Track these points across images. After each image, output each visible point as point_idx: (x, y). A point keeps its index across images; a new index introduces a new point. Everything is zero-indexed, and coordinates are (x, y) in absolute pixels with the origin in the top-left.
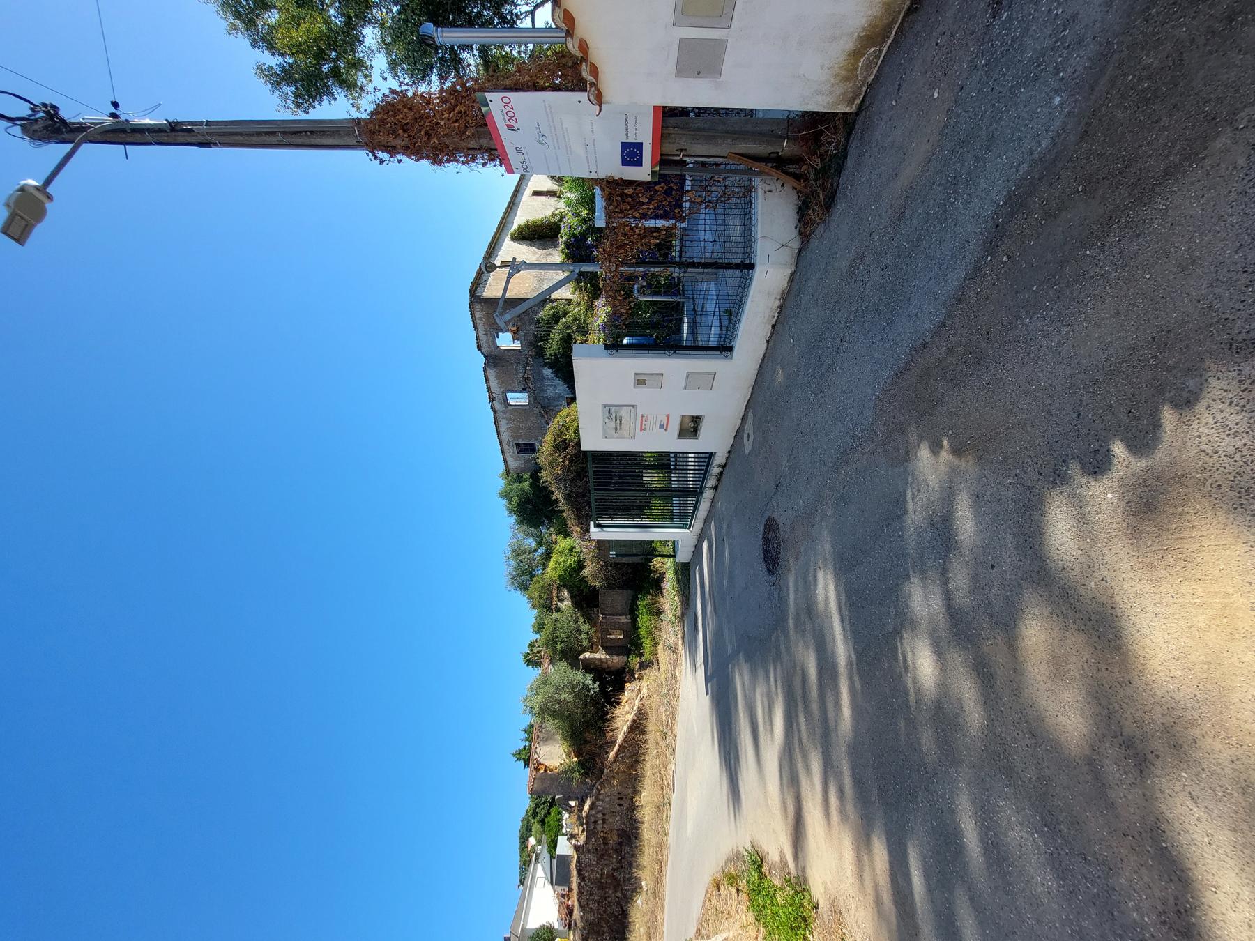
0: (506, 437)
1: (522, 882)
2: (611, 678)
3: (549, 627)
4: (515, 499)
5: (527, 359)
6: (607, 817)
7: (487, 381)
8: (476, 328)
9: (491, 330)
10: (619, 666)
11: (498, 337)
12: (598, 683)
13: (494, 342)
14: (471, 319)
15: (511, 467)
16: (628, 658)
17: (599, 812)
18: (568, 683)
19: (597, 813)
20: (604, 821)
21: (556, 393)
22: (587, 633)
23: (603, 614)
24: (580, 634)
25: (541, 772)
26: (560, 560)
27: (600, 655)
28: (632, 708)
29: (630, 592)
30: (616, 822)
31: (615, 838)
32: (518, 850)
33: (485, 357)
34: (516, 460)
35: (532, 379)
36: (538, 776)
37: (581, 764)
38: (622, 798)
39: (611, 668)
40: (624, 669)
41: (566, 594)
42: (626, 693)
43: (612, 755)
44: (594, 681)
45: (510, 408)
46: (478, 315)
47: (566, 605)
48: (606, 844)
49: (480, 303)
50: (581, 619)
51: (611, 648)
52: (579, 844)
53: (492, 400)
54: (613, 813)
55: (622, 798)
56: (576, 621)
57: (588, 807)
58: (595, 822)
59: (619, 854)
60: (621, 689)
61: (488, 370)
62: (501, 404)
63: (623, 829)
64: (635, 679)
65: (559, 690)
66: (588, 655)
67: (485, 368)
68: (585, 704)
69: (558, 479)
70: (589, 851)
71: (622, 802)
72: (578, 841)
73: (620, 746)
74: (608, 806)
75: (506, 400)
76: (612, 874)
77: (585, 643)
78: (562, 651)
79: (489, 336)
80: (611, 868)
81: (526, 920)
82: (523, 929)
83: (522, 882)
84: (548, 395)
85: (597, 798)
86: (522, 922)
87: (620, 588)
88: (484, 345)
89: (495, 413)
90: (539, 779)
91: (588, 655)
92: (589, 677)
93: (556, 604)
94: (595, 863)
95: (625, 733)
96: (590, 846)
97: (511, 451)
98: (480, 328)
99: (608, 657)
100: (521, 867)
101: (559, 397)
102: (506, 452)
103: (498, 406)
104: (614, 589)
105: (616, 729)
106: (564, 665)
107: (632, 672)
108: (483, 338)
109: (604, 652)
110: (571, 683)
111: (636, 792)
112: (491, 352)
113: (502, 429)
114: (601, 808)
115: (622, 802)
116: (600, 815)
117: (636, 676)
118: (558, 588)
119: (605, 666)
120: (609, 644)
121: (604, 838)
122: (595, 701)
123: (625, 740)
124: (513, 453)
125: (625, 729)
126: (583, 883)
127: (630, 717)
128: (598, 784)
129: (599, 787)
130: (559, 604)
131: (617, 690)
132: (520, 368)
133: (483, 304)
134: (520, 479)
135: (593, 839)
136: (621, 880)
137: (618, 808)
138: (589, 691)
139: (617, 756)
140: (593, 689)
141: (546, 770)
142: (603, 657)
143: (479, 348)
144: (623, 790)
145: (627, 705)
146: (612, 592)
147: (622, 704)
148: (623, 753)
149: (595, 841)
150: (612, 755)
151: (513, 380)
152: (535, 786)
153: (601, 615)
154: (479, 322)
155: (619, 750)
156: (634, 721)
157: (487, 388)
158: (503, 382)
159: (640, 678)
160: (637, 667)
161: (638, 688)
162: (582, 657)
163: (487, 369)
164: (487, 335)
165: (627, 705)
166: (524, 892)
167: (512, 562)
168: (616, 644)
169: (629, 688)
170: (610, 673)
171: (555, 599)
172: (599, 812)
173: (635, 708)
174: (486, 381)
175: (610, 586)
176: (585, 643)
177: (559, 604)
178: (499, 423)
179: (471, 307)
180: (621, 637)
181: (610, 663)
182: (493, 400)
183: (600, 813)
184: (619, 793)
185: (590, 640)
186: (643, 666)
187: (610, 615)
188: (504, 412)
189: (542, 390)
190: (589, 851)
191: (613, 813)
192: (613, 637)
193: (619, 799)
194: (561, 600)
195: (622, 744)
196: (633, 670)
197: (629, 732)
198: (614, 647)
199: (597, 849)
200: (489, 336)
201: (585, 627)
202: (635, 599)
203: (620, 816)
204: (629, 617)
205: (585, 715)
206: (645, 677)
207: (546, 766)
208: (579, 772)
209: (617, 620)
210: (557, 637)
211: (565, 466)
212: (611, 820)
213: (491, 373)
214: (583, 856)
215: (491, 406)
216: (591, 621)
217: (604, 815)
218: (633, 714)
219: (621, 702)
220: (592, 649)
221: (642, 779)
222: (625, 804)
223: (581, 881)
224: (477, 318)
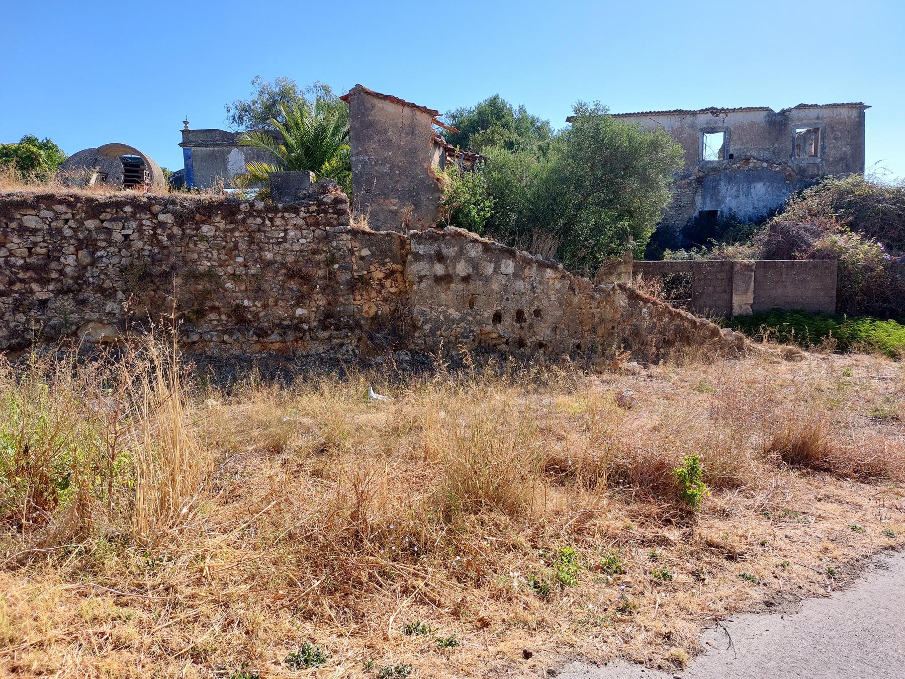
5: (780, 164)
6: (455, 286)
14: (814, 104)
19: (471, 261)
20: (445, 279)
21: (725, 197)
32: (543, 118)
33: (783, 112)
35: (746, 168)
46: (844, 112)
53: (713, 111)
61: (766, 113)
62: (707, 123)
67: (768, 109)
69: (40, 155)
71: (508, 320)
75: (713, 131)
79: (816, 121)
84: (723, 187)
88: (802, 113)
89: (694, 113)
98: (826, 113)
101: (718, 200)
103: (702, 119)
108: (813, 113)
112: (793, 121)
115: (508, 320)
132: (766, 155)
133: (857, 119)
134: (459, 128)
135: (365, 252)
137: (488, 313)
143: (801, 107)
144: (549, 319)
148: (651, 315)
149: (362, 258)
151: (747, 143)
154: (835, 112)
158: (744, 130)
164: (818, 118)
178: (673, 118)
182: (713, 113)
184: (537, 313)
188: (692, 126)
189: (730, 180)
200: (816, 121)
203: (463, 319)
213: (761, 117)
214: (300, 222)
217: (466, 279)
222: (500, 327)
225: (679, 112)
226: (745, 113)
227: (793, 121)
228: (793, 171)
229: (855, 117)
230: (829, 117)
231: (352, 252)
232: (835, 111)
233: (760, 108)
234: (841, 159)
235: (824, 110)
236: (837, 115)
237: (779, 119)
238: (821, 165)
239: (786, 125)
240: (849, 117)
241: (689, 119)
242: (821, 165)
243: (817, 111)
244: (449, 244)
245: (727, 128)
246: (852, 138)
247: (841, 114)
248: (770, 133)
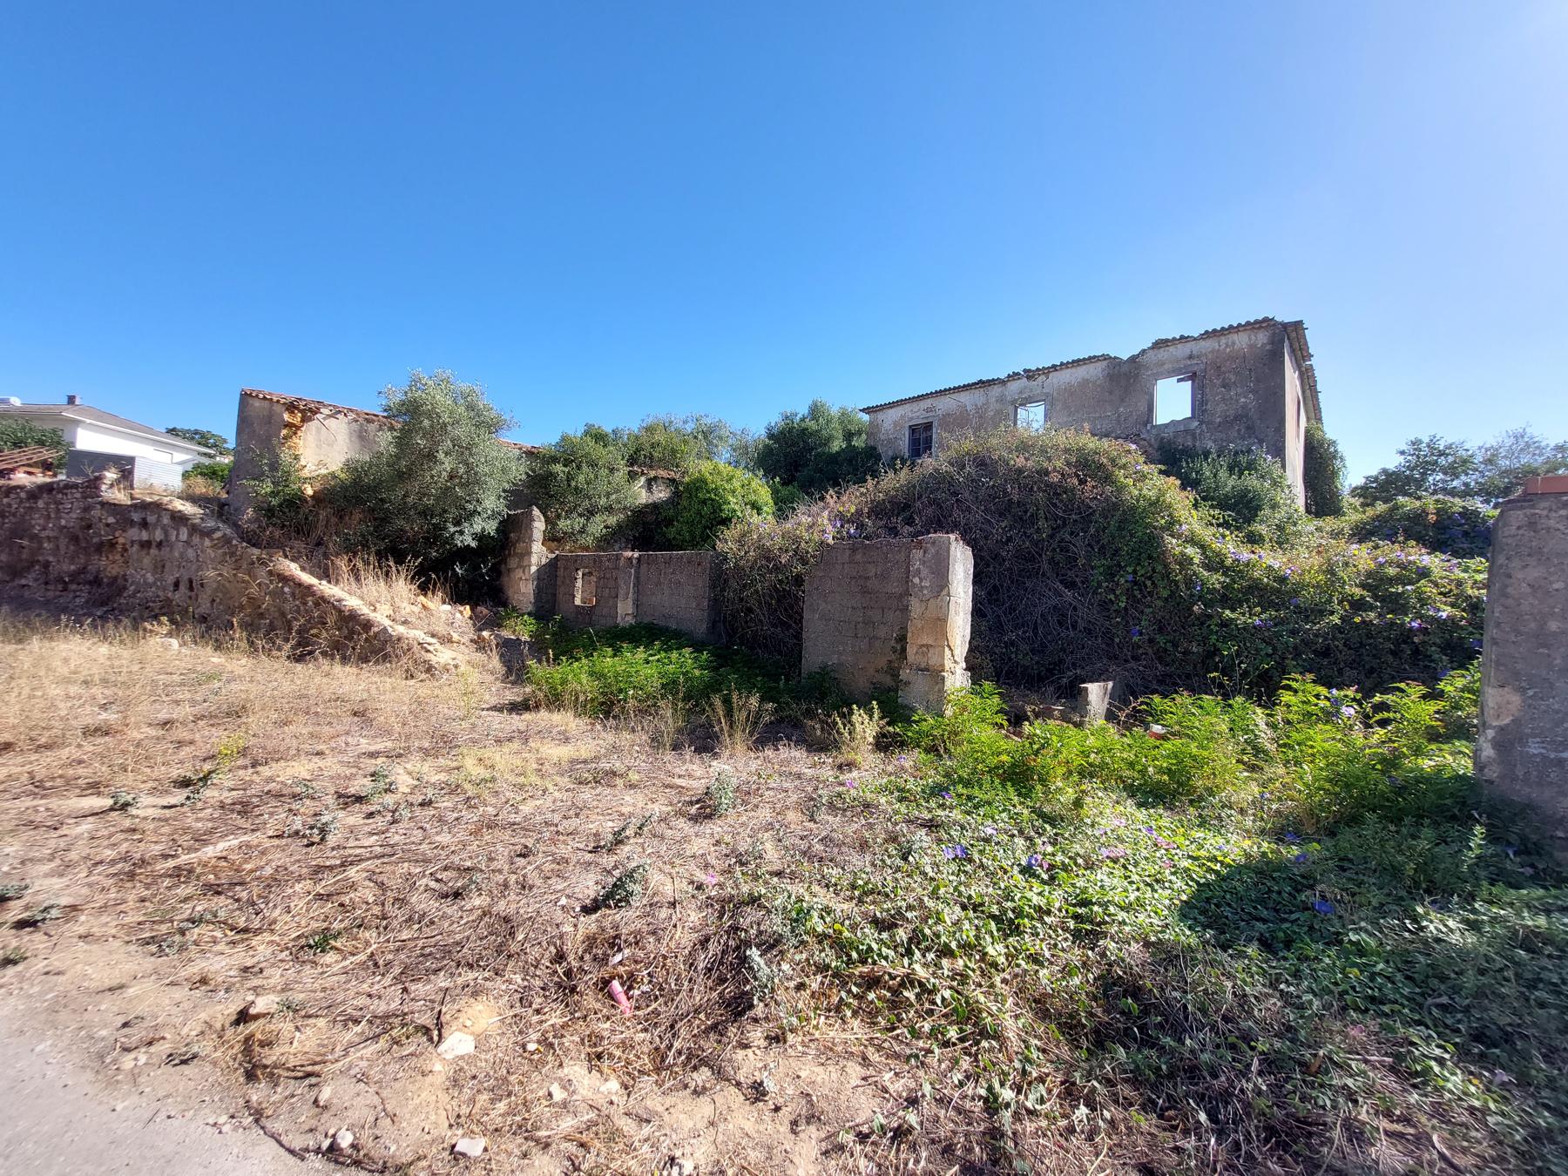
0: (946, 405)
1: (172, 432)
2: (482, 576)
3: (598, 451)
4: (812, 425)
6: (153, 551)
7: (1077, 363)
8: (1207, 335)
9: (1202, 366)
10: (510, 593)
11: (1179, 380)
12: (474, 544)
13: (1170, 374)
15: (880, 416)
16: (529, 614)
17: (166, 533)
18: (476, 474)
20: (146, 545)
22: (582, 531)
23: (639, 559)
24: (581, 515)
25: (286, 416)
26: (736, 484)
27: (539, 553)
28: (405, 623)
29: (701, 629)
30: (142, 573)
31: (114, 570)
33: (1133, 359)
34: (896, 424)
36: (277, 408)
37: (294, 502)
38: (191, 588)
39: (508, 576)
40: (505, 604)
41: (661, 494)
42: (447, 607)
43: (293, 569)
44: (481, 537)
45: (1011, 409)
46: (1242, 340)
47: (640, 494)
48: (99, 549)
49: (1272, 343)
50: (613, 520)
51: (552, 577)
52: (104, 487)
53: (1030, 375)
54: (160, 567)
55: (191, 588)
56: (609, 509)
57: (180, 507)
58: (144, 524)
59: (74, 576)
60: (458, 596)
63: (125, 588)
64: (480, 630)
65: (464, 450)
66: (539, 525)
67: (1105, 357)
68: (425, 513)
70: (87, 509)
71: (183, 588)
72: (112, 486)
73: (310, 587)
74: (176, 554)
75: (1026, 402)
76: (38, 561)
77: (563, 524)
78: (551, 475)
80: (51, 559)
81: (91, 427)
82: (76, 423)
83: (172, 432)
85: (194, 529)
86: (88, 421)
87: (716, 604)
88: (1163, 354)
89: (1002, 382)
90: (271, 410)
91: (539, 525)
92: (491, 527)
93: (643, 473)
94: (63, 522)
95: (339, 601)
96: (96, 513)
97: (917, 414)
99: (534, 569)
100: (196, 432)
102: (915, 404)
104: (713, 587)
105: (358, 579)
106: (519, 471)
107: (494, 623)
109: (544, 561)
110: (477, 482)
111: (177, 627)
113: (964, 398)
114: (174, 538)
115: (183, 588)
116: (158, 535)
117: (485, 634)
118: (673, 481)
119: (513, 563)
120: (561, 573)
121: (112, 545)
122: (435, 535)
123: (322, 600)
124: (912, 419)
125: (352, 602)
126: (23, 495)
127: (381, 617)
128: (228, 531)
129: (218, 535)
130: (643, 479)
131: (456, 585)
133: (1268, 347)
135: (111, 520)
136: (23, 582)
137: (171, 579)
138: (457, 523)
139: (285, 579)
140: (461, 533)
141: (288, 425)
142: (534, 559)
143: (1160, 344)
145: (416, 609)
146: (702, 582)
147: (422, 598)
148: (293, 595)
149: (108, 525)
150: (293, 569)
152: (257, 404)
153: (636, 554)
155: (300, 585)
156: (367, 625)
157: (1062, 364)
159: (480, 644)
160: (506, 634)
161: (456, 637)
162: (536, 512)
163: (1105, 363)
164: (1191, 357)
165: (416, 609)
166: (150, 430)
167: (689, 427)
168: (561, 590)
169: (458, 615)
170: (497, 572)
171: (652, 474)
172: (166, 533)
173: (401, 629)
174: (1079, 360)
175: (720, 577)
176: (563, 524)
177: (643, 479)
178: (977, 391)
179: (1266, 323)
180: (578, 602)
181: (519, 574)
182: (1028, 378)
183: (162, 537)
185: (569, 536)
186: (509, 650)
187: (637, 578)
188: (1001, 400)
190: (87, 509)
191: (160, 567)
192: (579, 583)
193: (191, 581)
194: (650, 482)
195: (313, 594)
196: (500, 626)
197: (340, 611)
198: (555, 586)
199: (89, 527)
201: (597, 526)
202: (698, 647)
203: (155, 583)
204: (630, 620)
205: (403, 509)
206: (479, 657)
207: (298, 428)
208: (274, 494)
209: (622, 592)
210: (579, 467)
211: (1047, 473)
212: (147, 561)
213: (1094, 371)
215: (1018, 374)
216: (611, 538)
217: (160, 545)
218: (387, 623)
219: (425, 595)
220: (552, 538)
221: (430, 593)
223: (27, 492)
224: (1235, 337)
225: (982, 384)
226: (1074, 370)
227: (1147, 369)
228: (1151, 445)
229: (1263, 345)
230: (1212, 352)
231: (100, 519)
232: (1223, 340)
233: (1090, 358)
234: (1237, 418)
235: (1202, 343)
236: (1227, 346)
237: (1125, 369)
238: (1198, 431)
239: (1137, 376)
240: (1251, 346)
241: (996, 391)
242: (1198, 431)
243: (1191, 345)
244: (153, 513)
245: (1047, 395)
246: (1258, 381)
247: (1234, 343)
248: (1111, 393)
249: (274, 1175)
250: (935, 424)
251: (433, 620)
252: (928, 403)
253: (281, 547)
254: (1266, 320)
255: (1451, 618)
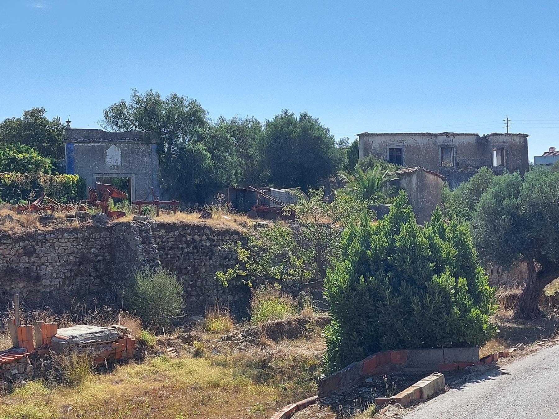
15: (371, 139)
33: (485, 137)
34: (381, 146)
88: (495, 139)
89: (436, 135)
102: (392, 137)
113: (418, 139)
124: (391, 144)
143: (495, 134)
182: (446, 136)
213: (472, 140)
227: (491, 143)
239: (487, 145)
249: (232, 418)
250: (404, 150)
251: (235, 215)
252: (400, 138)
253: (200, 167)
254: (496, 133)
255: (538, 262)
